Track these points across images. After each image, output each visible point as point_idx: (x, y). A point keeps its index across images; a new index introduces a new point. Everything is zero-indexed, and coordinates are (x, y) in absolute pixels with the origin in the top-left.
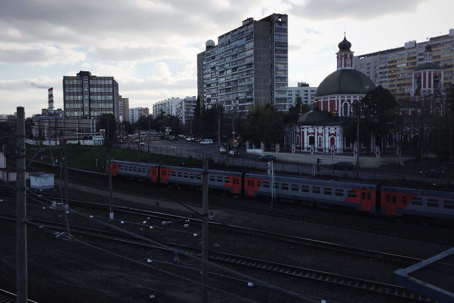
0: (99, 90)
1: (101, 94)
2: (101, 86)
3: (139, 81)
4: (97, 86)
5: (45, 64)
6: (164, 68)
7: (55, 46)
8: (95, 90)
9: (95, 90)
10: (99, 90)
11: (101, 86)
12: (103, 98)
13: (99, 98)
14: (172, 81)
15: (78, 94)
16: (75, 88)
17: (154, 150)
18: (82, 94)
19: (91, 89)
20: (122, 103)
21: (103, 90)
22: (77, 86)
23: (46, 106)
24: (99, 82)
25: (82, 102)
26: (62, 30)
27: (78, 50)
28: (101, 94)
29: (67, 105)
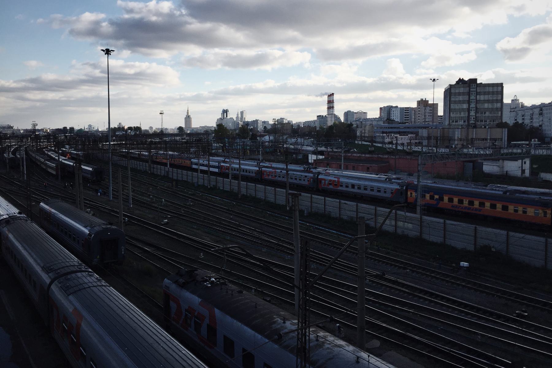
0: (486, 97)
1: (488, 101)
2: (488, 93)
3: (370, 80)
4: (485, 93)
5: (268, 68)
6: (396, 64)
7: (280, 49)
8: (482, 98)
9: (482, 98)
10: (486, 97)
11: (488, 93)
12: (490, 106)
13: (486, 105)
14: (411, 79)
15: (463, 102)
16: (481, 96)
17: (289, 167)
18: (477, 102)
19: (478, 96)
20: (431, 109)
21: (489, 97)
22: (463, 94)
23: (324, 111)
24: (487, 89)
25: (469, 110)
26: (291, 33)
27: (302, 51)
28: (488, 101)
29: (500, 115)
